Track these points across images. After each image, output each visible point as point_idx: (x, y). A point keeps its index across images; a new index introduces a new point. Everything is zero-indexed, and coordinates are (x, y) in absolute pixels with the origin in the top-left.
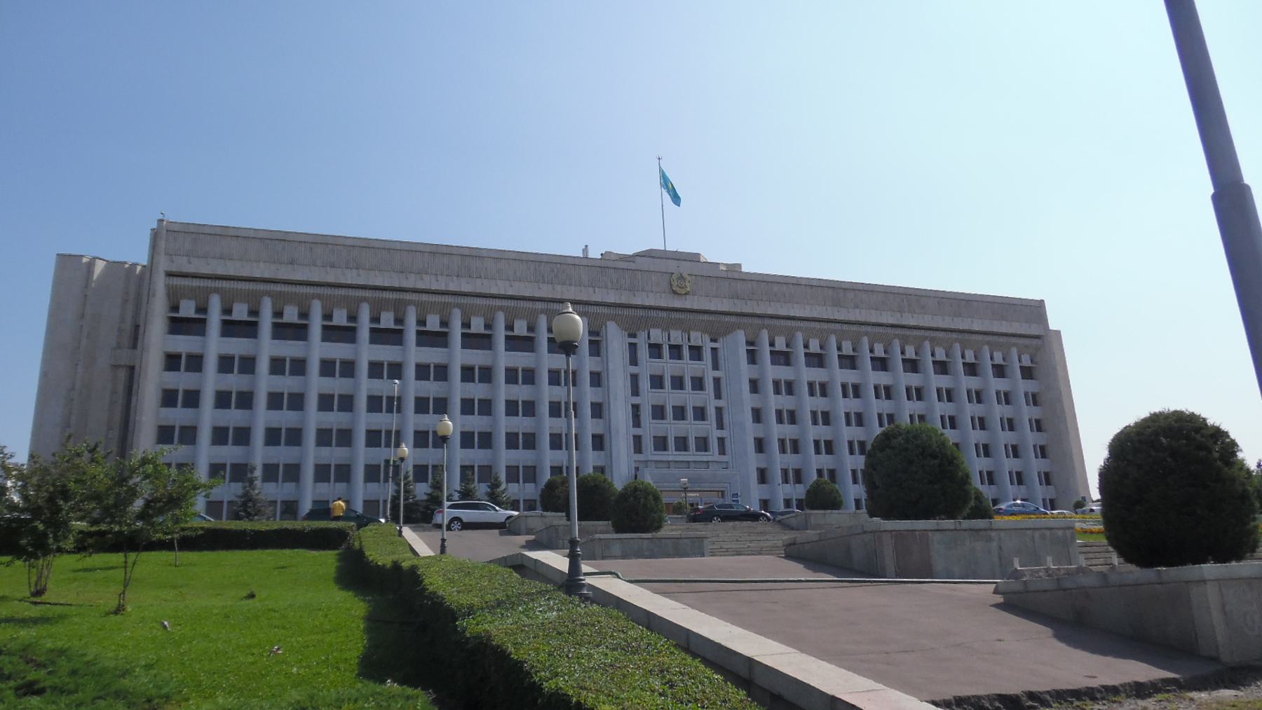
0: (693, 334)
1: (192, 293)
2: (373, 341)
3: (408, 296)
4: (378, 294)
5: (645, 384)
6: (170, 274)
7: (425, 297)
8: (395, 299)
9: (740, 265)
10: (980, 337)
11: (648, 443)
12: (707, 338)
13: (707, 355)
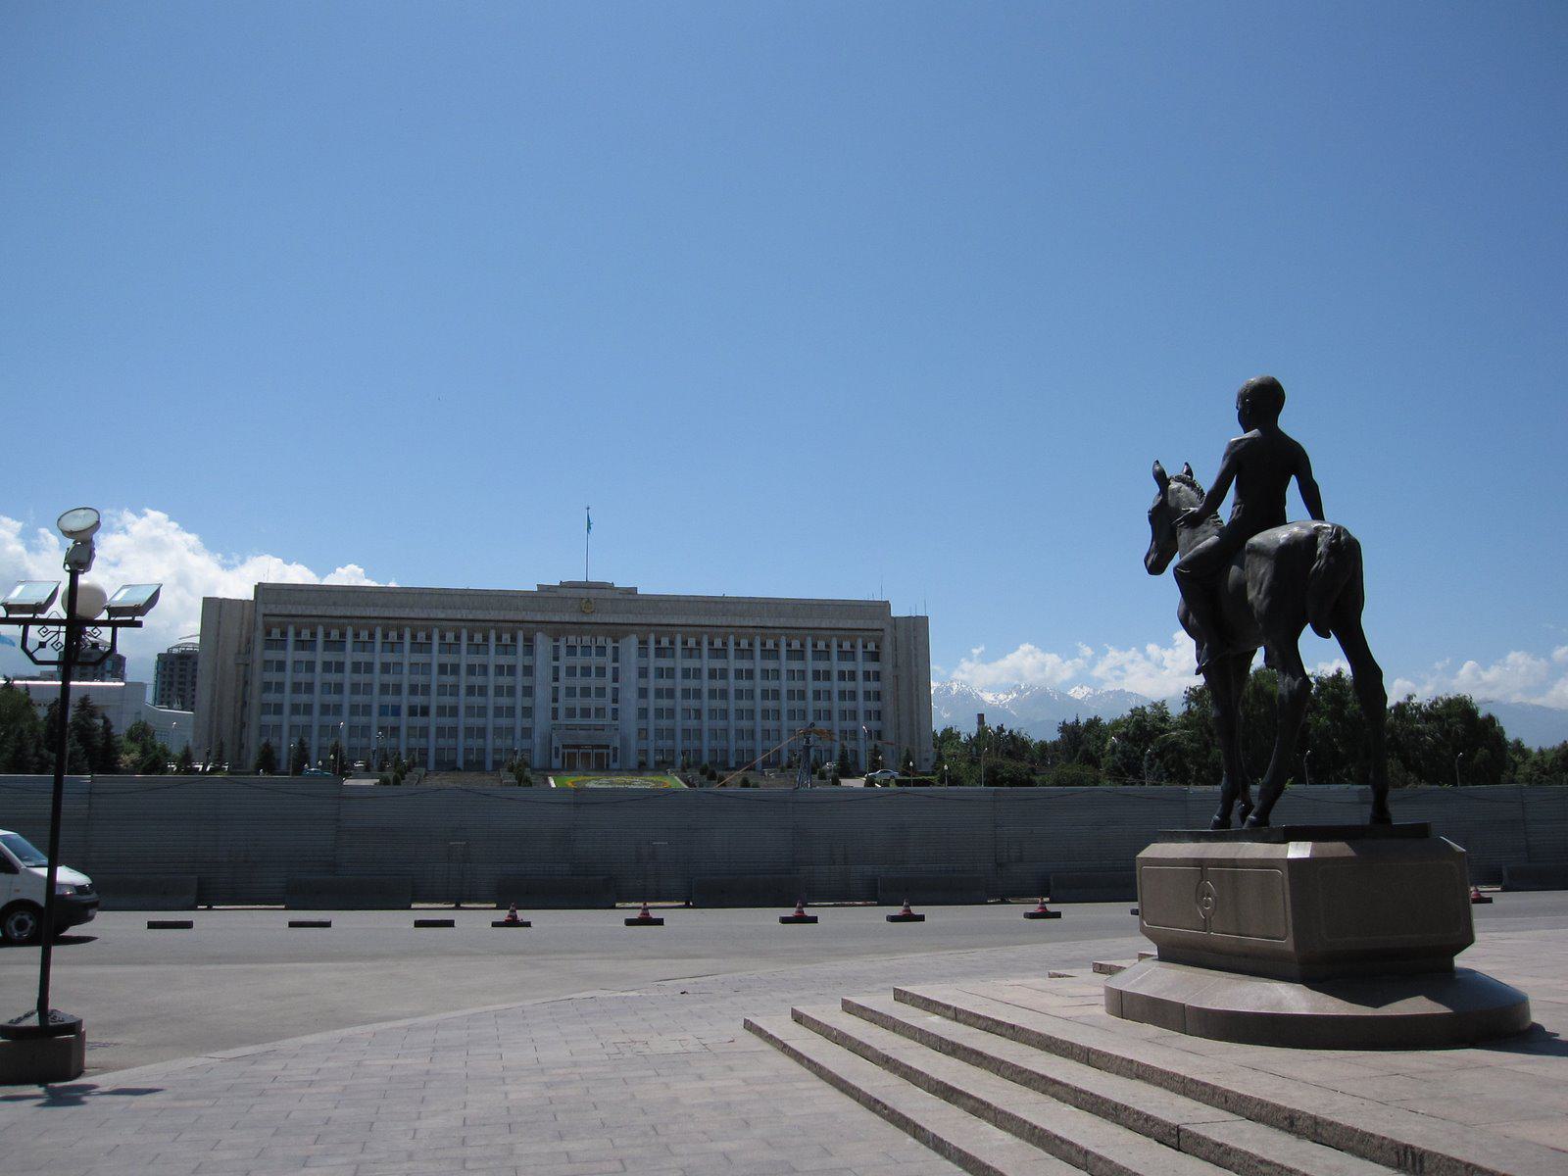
2: (296, 649)
3: (676, 629)
4: (386, 621)
5: (562, 674)
6: (265, 615)
7: (866, 633)
9: (886, 605)
10: (828, 632)
11: (562, 713)
12: (609, 640)
13: (609, 651)
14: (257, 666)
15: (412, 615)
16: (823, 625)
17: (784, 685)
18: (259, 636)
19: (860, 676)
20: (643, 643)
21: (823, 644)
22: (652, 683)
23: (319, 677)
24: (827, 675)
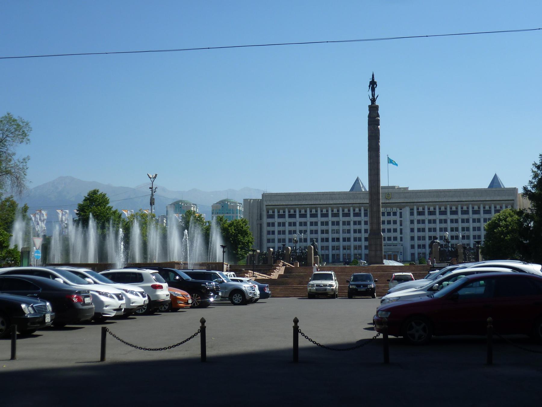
0: (388, 209)
1: (271, 209)
3: (318, 206)
8: (315, 207)
12: (398, 209)
13: (398, 214)
14: (265, 225)
15: (320, 203)
16: (487, 199)
17: (319, 228)
18: (265, 213)
19: (298, 224)
20: (412, 209)
21: (304, 211)
22: (416, 226)
23: (330, 227)
24: (295, 224)
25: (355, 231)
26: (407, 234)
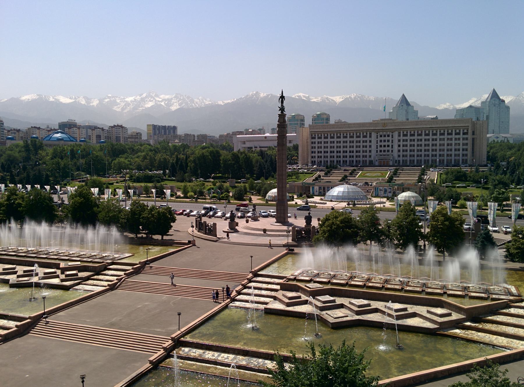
13: (391, 136)
22: (368, 144)
25: (340, 147)
26: (396, 148)
